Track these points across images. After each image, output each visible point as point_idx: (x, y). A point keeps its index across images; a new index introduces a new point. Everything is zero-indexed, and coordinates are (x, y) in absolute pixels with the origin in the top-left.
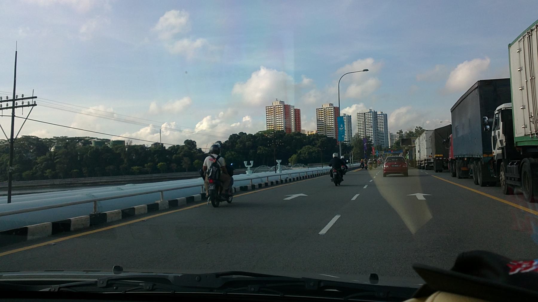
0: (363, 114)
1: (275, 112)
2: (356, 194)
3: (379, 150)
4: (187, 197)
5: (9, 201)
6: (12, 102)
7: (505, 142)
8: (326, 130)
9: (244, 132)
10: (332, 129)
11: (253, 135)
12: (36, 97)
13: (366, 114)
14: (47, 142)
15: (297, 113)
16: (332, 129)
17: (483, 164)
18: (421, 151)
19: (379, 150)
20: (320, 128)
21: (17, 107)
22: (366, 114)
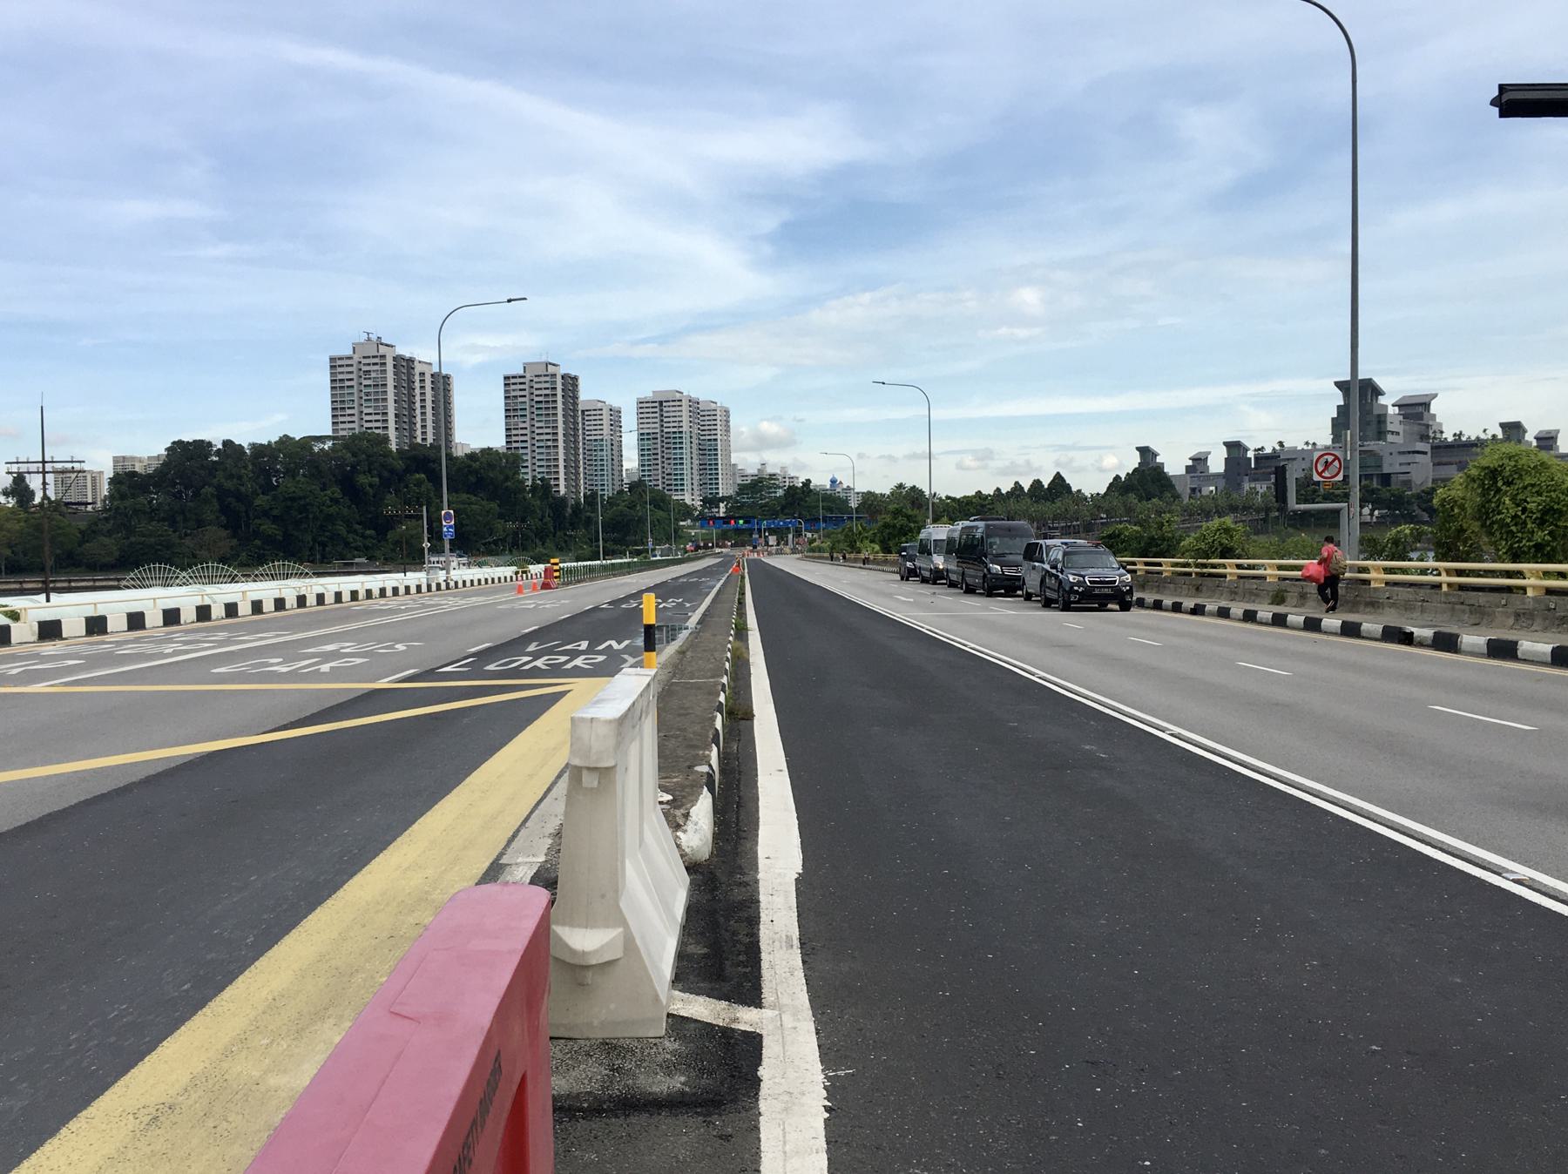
0: (657, 404)
1: (362, 412)
2: (618, 906)
3: (685, 408)
4: (92, 617)
5: (48, 600)
6: (47, 470)
7: (686, 628)
8: (363, 402)
9: (186, 440)
10: (643, 418)
11: (297, 439)
12: (84, 462)
13: (664, 404)
14: (491, 466)
15: (442, 384)
16: (643, 418)
17: (281, 660)
18: (1249, 626)
19: (685, 408)
20: (649, 423)
21: (47, 472)
22: (664, 404)
